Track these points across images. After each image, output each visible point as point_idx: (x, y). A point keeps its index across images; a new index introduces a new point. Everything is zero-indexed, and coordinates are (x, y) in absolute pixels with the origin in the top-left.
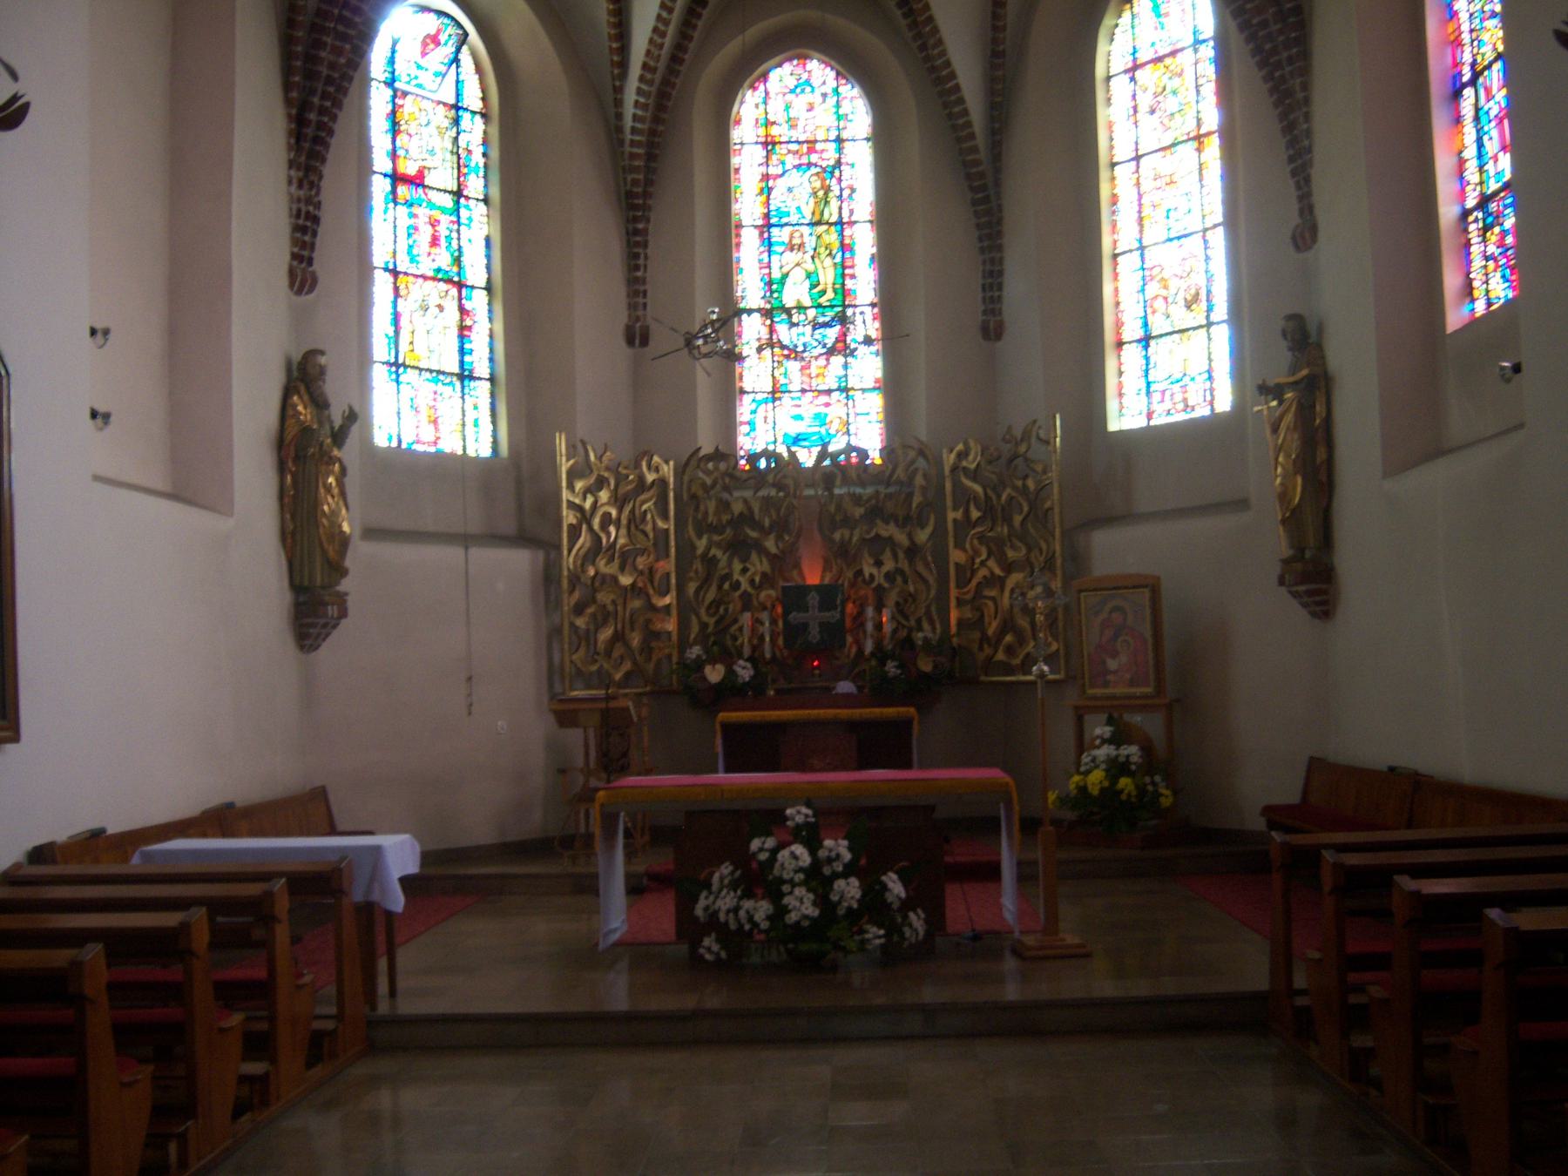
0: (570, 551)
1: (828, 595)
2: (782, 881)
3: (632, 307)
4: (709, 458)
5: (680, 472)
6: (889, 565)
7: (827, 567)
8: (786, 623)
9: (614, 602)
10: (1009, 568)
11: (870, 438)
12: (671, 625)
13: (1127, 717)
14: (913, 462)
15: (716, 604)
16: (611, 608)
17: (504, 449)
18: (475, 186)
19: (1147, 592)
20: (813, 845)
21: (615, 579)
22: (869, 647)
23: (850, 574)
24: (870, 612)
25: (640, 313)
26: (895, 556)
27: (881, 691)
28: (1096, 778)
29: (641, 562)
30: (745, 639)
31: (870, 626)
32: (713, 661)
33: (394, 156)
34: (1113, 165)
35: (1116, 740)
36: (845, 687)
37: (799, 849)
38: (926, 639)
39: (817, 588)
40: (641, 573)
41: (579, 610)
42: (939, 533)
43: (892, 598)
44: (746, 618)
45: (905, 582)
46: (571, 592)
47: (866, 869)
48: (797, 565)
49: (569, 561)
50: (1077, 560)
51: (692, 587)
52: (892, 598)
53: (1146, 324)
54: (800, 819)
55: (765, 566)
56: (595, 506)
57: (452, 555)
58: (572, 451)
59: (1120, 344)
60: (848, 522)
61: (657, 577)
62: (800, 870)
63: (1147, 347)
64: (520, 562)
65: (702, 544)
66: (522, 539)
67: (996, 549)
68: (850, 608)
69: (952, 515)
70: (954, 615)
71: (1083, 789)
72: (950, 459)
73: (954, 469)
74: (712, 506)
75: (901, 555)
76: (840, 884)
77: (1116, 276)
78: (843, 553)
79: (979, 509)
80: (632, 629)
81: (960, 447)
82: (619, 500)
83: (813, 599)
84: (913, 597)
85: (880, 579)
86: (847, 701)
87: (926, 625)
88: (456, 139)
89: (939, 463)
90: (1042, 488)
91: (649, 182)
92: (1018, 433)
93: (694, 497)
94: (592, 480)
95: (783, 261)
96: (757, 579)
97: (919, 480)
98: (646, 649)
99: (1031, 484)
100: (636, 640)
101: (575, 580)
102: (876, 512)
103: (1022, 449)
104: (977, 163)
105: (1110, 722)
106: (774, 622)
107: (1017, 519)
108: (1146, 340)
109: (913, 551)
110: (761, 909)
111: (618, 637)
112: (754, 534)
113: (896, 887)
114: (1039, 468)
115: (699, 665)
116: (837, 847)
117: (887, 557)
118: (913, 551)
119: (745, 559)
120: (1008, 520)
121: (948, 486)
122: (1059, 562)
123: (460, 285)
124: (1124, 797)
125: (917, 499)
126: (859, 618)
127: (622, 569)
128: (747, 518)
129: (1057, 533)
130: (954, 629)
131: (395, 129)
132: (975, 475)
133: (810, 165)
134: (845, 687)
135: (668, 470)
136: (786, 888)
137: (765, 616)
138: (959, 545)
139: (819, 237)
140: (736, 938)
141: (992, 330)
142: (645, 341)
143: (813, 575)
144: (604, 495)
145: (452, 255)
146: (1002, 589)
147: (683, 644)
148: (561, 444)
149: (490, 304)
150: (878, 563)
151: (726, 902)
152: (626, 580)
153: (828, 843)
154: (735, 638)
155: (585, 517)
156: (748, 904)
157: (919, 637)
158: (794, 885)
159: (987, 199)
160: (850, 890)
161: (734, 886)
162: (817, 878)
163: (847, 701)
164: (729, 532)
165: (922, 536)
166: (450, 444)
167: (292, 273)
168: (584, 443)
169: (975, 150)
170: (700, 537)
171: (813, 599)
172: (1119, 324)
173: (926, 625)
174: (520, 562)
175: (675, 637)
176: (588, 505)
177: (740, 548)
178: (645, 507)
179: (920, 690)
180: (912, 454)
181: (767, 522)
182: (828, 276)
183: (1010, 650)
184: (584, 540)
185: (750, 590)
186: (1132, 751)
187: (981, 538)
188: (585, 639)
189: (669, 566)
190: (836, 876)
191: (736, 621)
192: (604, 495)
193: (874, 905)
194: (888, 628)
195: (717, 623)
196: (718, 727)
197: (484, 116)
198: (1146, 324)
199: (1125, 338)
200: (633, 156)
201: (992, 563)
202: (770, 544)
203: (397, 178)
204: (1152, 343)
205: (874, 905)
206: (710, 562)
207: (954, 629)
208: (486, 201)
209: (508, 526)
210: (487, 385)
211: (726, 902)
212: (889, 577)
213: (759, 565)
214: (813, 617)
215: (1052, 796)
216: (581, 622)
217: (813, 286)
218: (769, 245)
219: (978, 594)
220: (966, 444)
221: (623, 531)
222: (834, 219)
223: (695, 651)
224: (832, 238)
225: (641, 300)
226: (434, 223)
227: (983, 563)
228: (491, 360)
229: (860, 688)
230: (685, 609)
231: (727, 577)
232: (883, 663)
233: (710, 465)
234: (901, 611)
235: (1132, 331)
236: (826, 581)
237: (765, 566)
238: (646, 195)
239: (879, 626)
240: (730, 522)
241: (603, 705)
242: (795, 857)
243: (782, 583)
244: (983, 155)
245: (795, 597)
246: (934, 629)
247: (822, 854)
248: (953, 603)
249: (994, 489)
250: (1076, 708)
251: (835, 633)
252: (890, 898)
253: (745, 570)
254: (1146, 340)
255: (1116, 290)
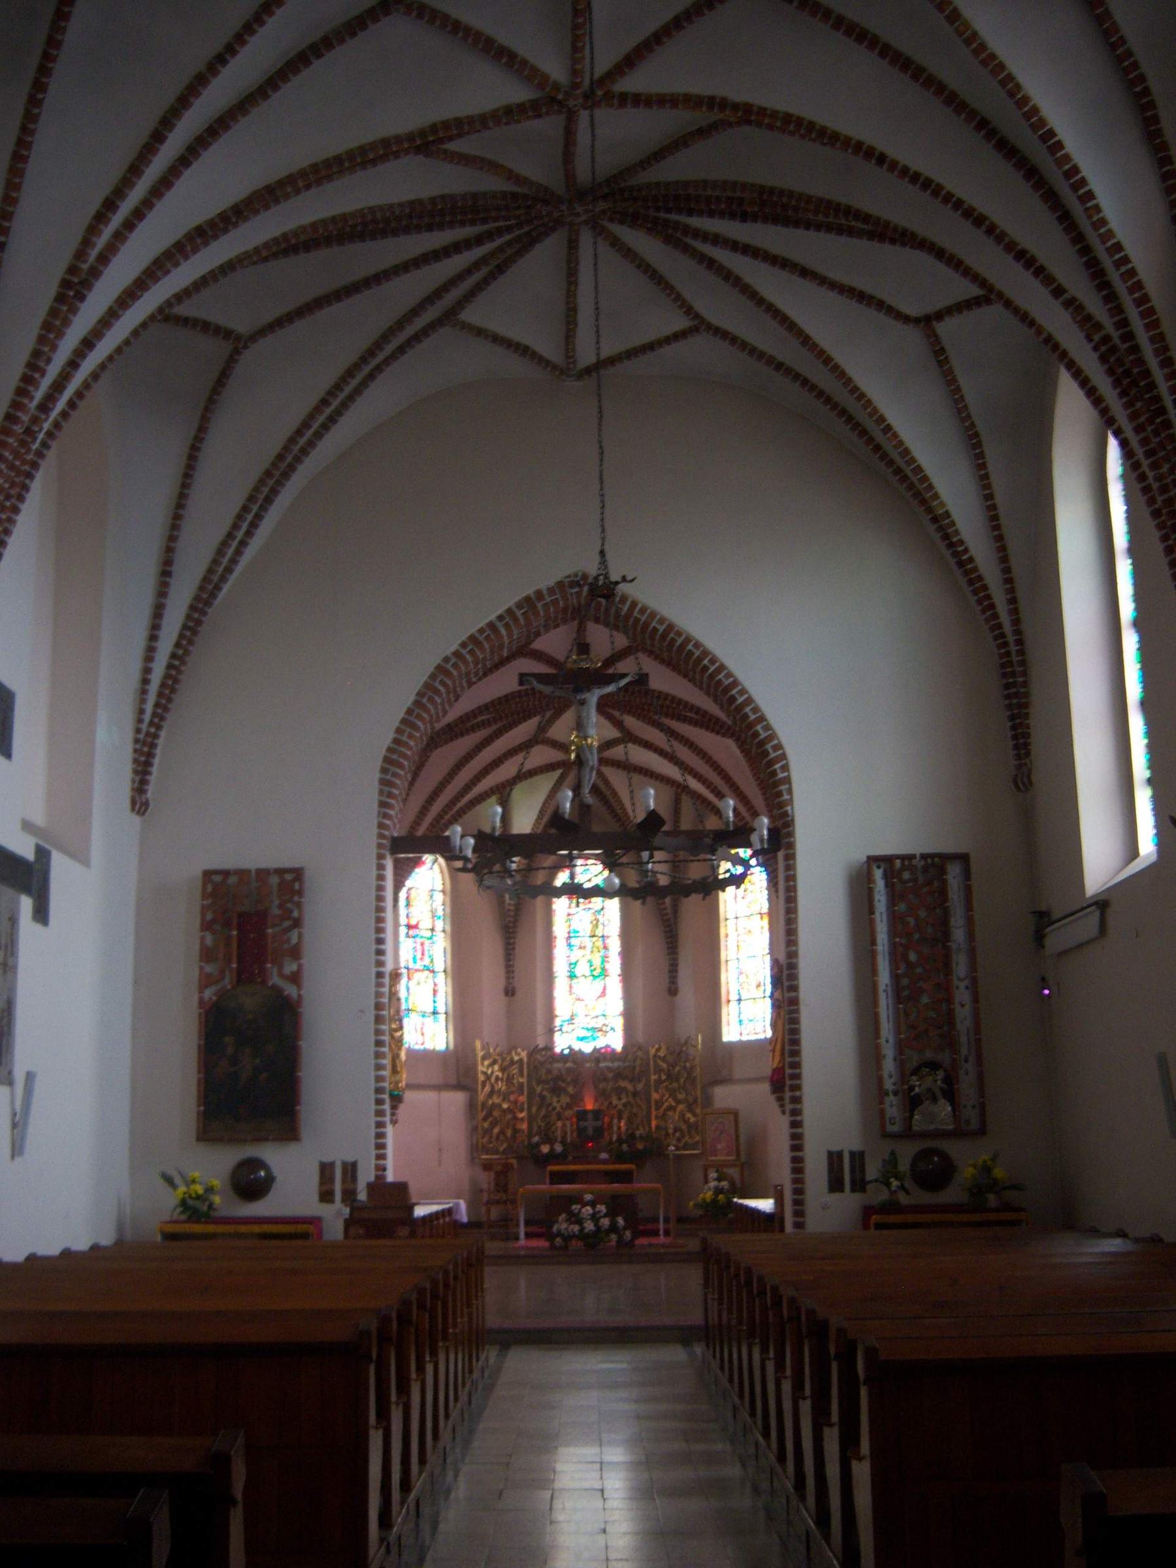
0: (482, 1091)
1: (597, 1114)
2: (583, 1219)
3: (508, 978)
4: (543, 1049)
5: (530, 1055)
6: (624, 1101)
7: (596, 1100)
8: (578, 1126)
9: (500, 1116)
10: (678, 1102)
11: (616, 1042)
12: (524, 1126)
13: (725, 1170)
14: (636, 1052)
15: (545, 1117)
16: (499, 1118)
17: (451, 1046)
18: (439, 925)
19: (732, 1117)
20: (593, 1206)
21: (500, 1106)
22: (615, 1138)
23: (606, 1104)
24: (615, 1121)
25: (511, 981)
26: (627, 1096)
27: (619, 1158)
28: (709, 1195)
29: (512, 1098)
30: (559, 1133)
31: (615, 1128)
32: (545, 1143)
33: (408, 916)
34: (727, 919)
35: (719, 1179)
36: (604, 1156)
37: (589, 1208)
38: (640, 1134)
39: (592, 1111)
40: (512, 1102)
41: (485, 1119)
42: (647, 1085)
43: (626, 1115)
44: (559, 1124)
45: (632, 1108)
46: (482, 1111)
47: (611, 1214)
48: (582, 1100)
49: (481, 1097)
50: (708, 1100)
51: (534, 1109)
52: (626, 1115)
53: (739, 994)
54: (589, 1198)
55: (568, 1100)
56: (492, 1073)
57: (431, 1095)
58: (483, 1048)
59: (729, 1001)
60: (605, 1080)
61: (519, 1104)
62: (589, 1215)
63: (739, 1003)
64: (458, 1099)
65: (539, 1089)
66: (459, 1087)
67: (673, 1093)
68: (606, 1119)
69: (653, 1077)
70: (654, 1123)
71: (704, 1200)
72: (653, 1051)
73: (655, 1056)
74: (544, 1071)
75: (630, 1095)
76: (602, 1220)
77: (727, 970)
78: (602, 1095)
79: (665, 1074)
80: (508, 1128)
81: (657, 1046)
82: (503, 1069)
83: (590, 1116)
84: (635, 1115)
85: (620, 1107)
86: (605, 1162)
87: (641, 1128)
88: (431, 905)
89: (647, 1053)
90: (693, 1067)
91: (515, 921)
92: (683, 1041)
93: (536, 1067)
94: (491, 1060)
95: (576, 954)
96: (564, 1106)
97: (638, 1062)
98: (514, 1137)
99: (688, 1064)
100: (509, 1133)
101: (484, 1105)
102: (619, 1075)
103: (684, 1049)
104: (667, 914)
105: (717, 1171)
106: (572, 1125)
107: (682, 1080)
108: (739, 1000)
109: (635, 1094)
110: (576, 1228)
111: (502, 1132)
112: (563, 1085)
113: (620, 1221)
114: (691, 1058)
115: (537, 1145)
116: (602, 1208)
117: (623, 1096)
118: (635, 1094)
119: (559, 1096)
120: (677, 1080)
121: (652, 1063)
122: (699, 1101)
123: (433, 971)
124: (721, 1203)
125: (637, 1069)
126: (610, 1125)
127: (504, 1100)
128: (560, 1078)
129: (699, 1087)
130: (653, 1129)
131: (408, 905)
132: (664, 1059)
133: (589, 909)
134: (604, 1156)
135: (524, 1054)
136: (584, 1221)
137: (568, 1123)
138: (656, 1091)
139: (594, 943)
140: (567, 1238)
141: (673, 991)
142: (513, 994)
143: (590, 1105)
144: (496, 1067)
145: (512, 1048)
146: (675, 1112)
147: (530, 1136)
148: (478, 1044)
149: (446, 978)
150: (620, 1099)
151: (564, 1226)
152: (505, 1106)
153: (598, 1206)
154: (553, 1133)
155: (488, 1077)
156: (572, 1226)
157: (638, 1133)
158: (587, 1219)
159: (671, 931)
160: (605, 1222)
161: (566, 1221)
162: (595, 1217)
163: (605, 1162)
164: (552, 1083)
165: (640, 1087)
166: (429, 1046)
167: (133, 803)
168: (488, 1044)
169: (665, 909)
170: (538, 1086)
171: (590, 1116)
172: (728, 993)
173: (641, 1128)
174: (458, 1099)
175: (526, 1131)
176: (489, 1072)
177: (556, 1091)
178: (514, 1072)
179: (638, 1157)
180: (635, 1049)
181: (569, 1079)
182: (597, 962)
183: (679, 1140)
184: (487, 1088)
185: (561, 1110)
186: (725, 1184)
187: (666, 1088)
188: (487, 1132)
189: (523, 1099)
190: (601, 1217)
191: (554, 1125)
192: (496, 1067)
193: (613, 1228)
194: (623, 1129)
195: (546, 1125)
196: (548, 1174)
197: (443, 891)
198: (739, 994)
199: (731, 998)
200: (509, 910)
201: (670, 1099)
202: (571, 1090)
203: (409, 927)
204: (742, 1002)
205: (613, 1228)
206: (543, 1098)
207: (653, 1129)
208: (444, 931)
209: (453, 1080)
210: (445, 1016)
211: (564, 1226)
212: (625, 1105)
213: (565, 1100)
214: (590, 1124)
215: (691, 1204)
216: (486, 1125)
217: (591, 966)
218: (569, 945)
219: (664, 1114)
220: (659, 1045)
221: (504, 1083)
222: (600, 935)
223: (536, 1139)
224: (600, 943)
225: (512, 975)
226: (422, 944)
227: (667, 1100)
228: (446, 1004)
229: (611, 1156)
230: (531, 1119)
231: (550, 1104)
232: (620, 1145)
233: (543, 1053)
234: (630, 1121)
235: (733, 997)
236: (596, 1108)
237: (568, 1100)
238: (514, 927)
239: (619, 1128)
240: (551, 1079)
241: (504, 1161)
242: (587, 1210)
243: (576, 1109)
244: (669, 911)
245: (582, 1115)
246: (644, 1129)
247: (597, 1210)
248: (653, 1118)
249: (672, 1066)
250: (705, 1166)
251: (599, 1132)
252: (619, 1225)
253: (559, 1101)
254: (739, 1000)
255: (727, 978)
